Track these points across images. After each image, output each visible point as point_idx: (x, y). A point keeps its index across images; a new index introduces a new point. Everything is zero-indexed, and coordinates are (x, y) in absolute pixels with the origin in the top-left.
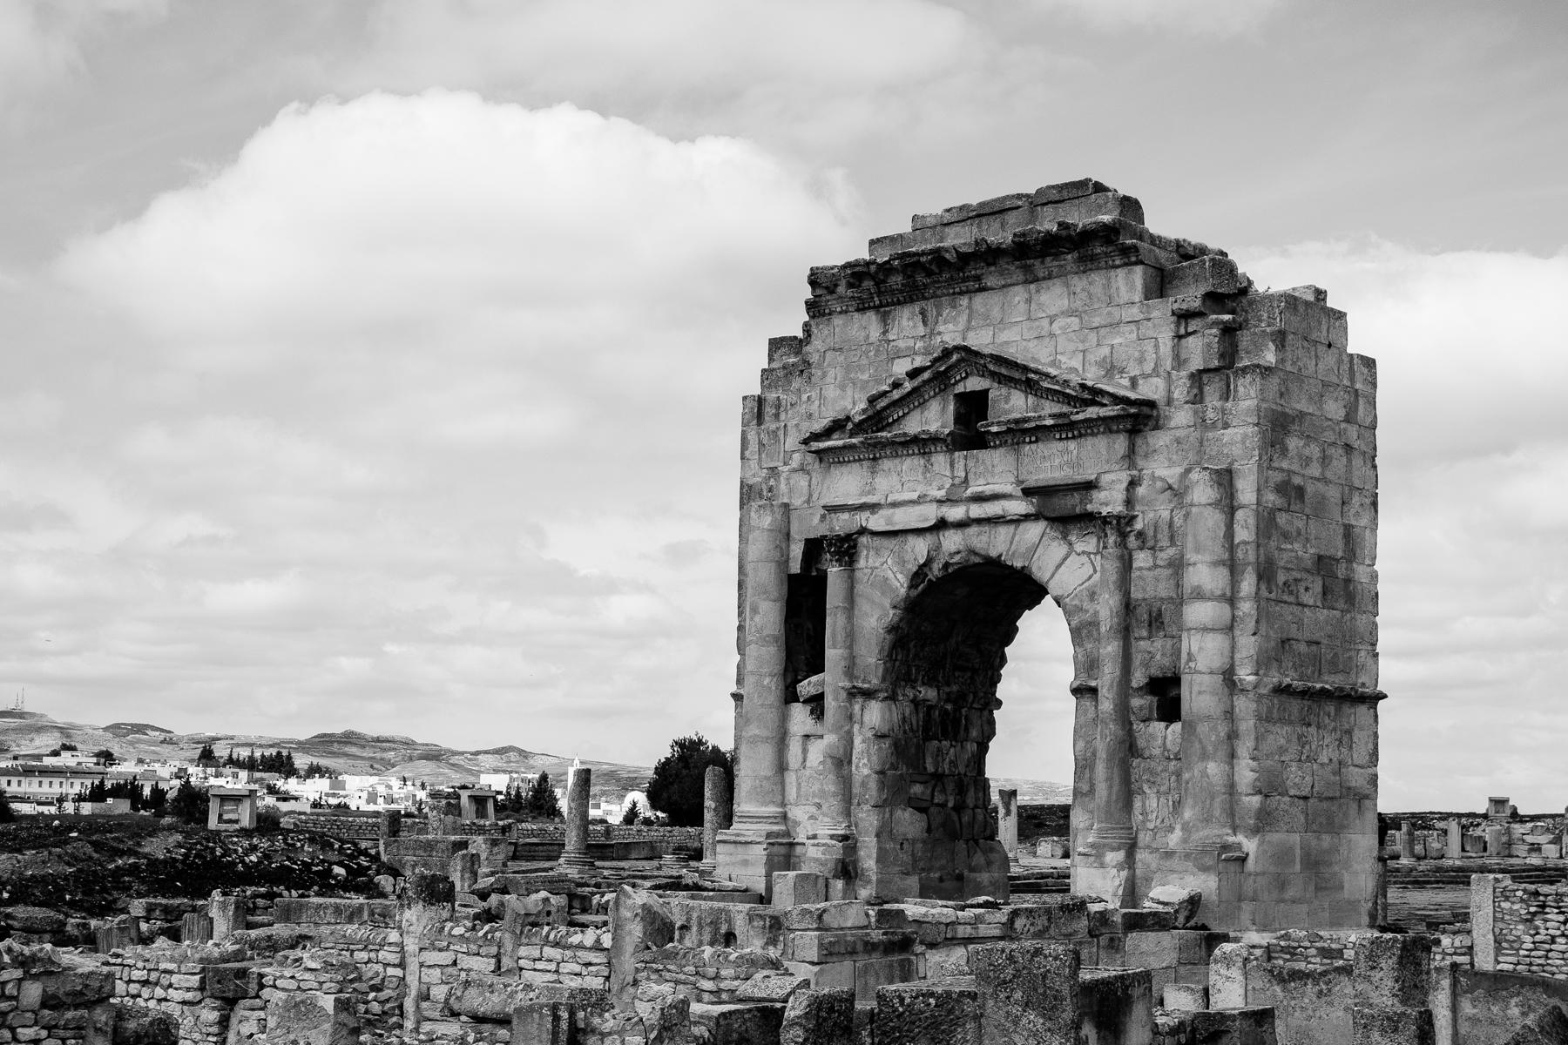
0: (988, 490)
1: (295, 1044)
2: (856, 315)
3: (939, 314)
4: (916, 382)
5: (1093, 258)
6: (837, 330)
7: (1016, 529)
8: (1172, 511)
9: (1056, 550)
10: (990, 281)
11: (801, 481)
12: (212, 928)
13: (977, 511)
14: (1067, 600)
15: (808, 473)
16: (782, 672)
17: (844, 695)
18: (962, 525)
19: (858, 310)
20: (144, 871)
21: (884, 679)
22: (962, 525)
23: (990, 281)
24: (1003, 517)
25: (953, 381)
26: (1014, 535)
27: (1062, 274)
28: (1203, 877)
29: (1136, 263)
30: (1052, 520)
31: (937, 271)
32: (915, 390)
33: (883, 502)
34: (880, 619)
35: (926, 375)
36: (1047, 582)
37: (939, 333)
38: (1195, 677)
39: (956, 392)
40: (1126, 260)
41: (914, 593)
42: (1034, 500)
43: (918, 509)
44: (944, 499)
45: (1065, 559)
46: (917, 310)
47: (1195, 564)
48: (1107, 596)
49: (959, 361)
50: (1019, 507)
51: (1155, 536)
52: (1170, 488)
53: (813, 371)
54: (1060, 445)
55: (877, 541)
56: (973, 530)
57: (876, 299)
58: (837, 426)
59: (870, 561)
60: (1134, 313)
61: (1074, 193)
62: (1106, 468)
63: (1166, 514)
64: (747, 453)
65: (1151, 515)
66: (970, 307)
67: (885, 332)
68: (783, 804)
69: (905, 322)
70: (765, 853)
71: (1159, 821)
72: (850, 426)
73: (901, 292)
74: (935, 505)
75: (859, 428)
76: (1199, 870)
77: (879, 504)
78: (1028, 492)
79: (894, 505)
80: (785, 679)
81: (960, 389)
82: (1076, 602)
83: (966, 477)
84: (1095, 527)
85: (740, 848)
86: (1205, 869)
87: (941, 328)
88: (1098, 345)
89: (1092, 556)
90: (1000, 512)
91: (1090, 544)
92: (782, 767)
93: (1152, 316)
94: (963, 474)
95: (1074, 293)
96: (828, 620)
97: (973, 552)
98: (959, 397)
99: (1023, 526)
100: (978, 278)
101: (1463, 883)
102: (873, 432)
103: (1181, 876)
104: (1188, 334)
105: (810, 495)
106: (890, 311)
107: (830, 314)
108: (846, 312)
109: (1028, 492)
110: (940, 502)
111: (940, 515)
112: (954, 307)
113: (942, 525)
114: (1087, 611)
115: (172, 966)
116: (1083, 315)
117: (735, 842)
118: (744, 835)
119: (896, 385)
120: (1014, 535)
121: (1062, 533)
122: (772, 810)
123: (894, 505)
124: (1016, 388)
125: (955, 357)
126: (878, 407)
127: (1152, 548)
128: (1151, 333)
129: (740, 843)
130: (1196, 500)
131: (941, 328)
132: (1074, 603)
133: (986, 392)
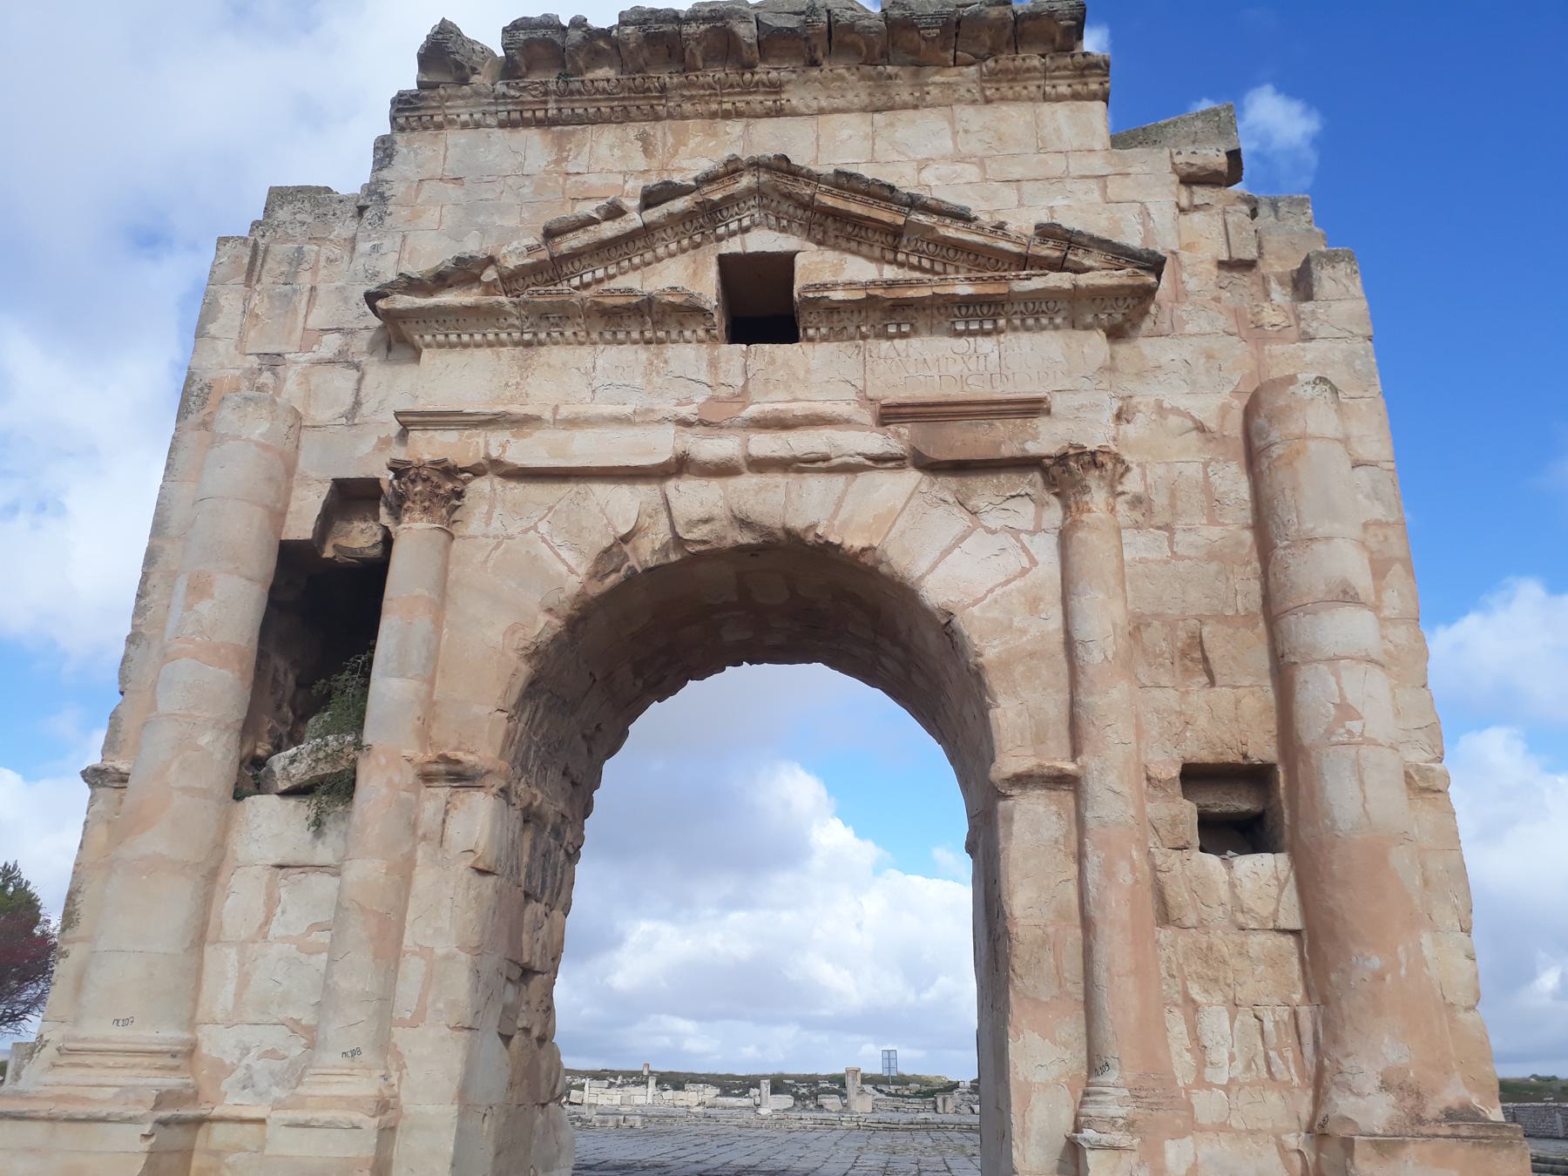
0: (799, 409)
2: (499, 132)
3: (680, 143)
4: (654, 214)
5: (1014, 76)
6: (451, 151)
7: (848, 485)
8: (1206, 465)
9: (946, 522)
10: (795, 97)
11: (341, 382)
13: (766, 444)
14: (976, 610)
15: (357, 367)
16: (239, 725)
17: (410, 775)
18: (723, 470)
19: (502, 125)
20: (14, 975)
21: (502, 756)
22: (723, 470)
23: (795, 97)
24: (826, 459)
25: (721, 230)
26: (845, 493)
27: (949, 100)
29: (1093, 97)
30: (932, 467)
31: (701, 67)
32: (647, 230)
33: (547, 415)
34: (512, 630)
35: (680, 204)
36: (922, 577)
38: (1364, 750)
40: (1079, 88)
41: (596, 589)
43: (628, 435)
44: (693, 419)
45: (963, 538)
47: (1328, 539)
48: (1101, 596)
49: (751, 192)
50: (875, 442)
51: (1173, 506)
52: (1201, 428)
53: (391, 209)
55: (517, 490)
56: (748, 482)
57: (552, 105)
58: (463, 272)
59: (496, 523)
60: (1097, 164)
62: (1067, 383)
63: (1193, 471)
64: (212, 329)
65: (1160, 470)
68: (191, 1023)
69: (603, 150)
70: (146, 1145)
71: (1239, 1064)
73: (609, 95)
74: (671, 429)
75: (511, 281)
77: (538, 419)
78: (889, 415)
79: (573, 423)
80: (241, 747)
81: (733, 246)
82: (995, 613)
84: (1032, 484)
85: (67, 1133)
88: (1020, 205)
89: (1023, 537)
91: (1024, 514)
92: (201, 935)
93: (1130, 170)
97: (744, 523)
98: (722, 259)
99: (863, 478)
100: (776, 88)
101: (1545, 1161)
104: (1197, 208)
105: (357, 404)
107: (440, 127)
108: (478, 125)
109: (889, 415)
110: (685, 423)
111: (680, 450)
113: (681, 466)
117: (51, 1119)
118: (85, 1100)
119: (615, 211)
120: (845, 493)
122: (169, 1034)
123: (573, 423)
125: (746, 181)
127: (1167, 527)
129: (71, 1120)
130: (1312, 428)
132: (990, 615)
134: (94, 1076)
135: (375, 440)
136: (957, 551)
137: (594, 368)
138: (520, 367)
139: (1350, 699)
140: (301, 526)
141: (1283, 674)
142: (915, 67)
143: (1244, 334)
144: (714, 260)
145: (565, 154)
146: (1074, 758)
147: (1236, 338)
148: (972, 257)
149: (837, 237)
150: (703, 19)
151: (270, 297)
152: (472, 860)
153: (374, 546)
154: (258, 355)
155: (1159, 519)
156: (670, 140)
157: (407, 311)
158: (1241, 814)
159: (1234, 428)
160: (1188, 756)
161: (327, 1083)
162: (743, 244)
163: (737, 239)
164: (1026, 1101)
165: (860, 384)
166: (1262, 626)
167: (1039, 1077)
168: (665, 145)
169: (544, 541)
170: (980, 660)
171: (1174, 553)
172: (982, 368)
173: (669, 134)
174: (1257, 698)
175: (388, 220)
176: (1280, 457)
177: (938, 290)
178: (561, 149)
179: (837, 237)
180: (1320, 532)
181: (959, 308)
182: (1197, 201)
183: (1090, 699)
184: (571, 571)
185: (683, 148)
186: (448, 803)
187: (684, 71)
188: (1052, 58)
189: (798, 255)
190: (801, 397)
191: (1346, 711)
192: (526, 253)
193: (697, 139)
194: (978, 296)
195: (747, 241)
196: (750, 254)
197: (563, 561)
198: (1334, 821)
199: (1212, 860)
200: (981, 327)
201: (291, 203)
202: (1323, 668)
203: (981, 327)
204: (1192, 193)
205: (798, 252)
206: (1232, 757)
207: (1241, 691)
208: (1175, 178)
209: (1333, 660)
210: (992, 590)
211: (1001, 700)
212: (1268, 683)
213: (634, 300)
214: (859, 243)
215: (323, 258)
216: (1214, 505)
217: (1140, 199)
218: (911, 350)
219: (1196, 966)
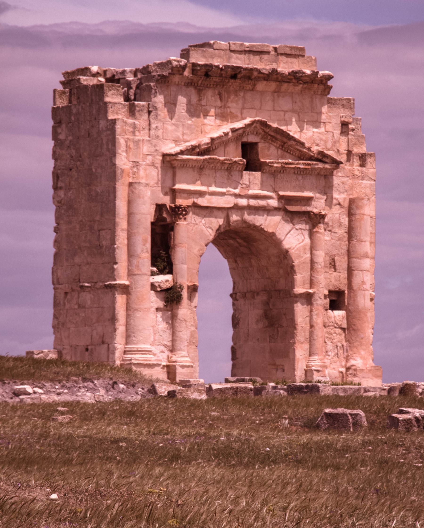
1: (372, 527)
3: (229, 97)
9: (288, 227)
13: (253, 202)
28: (376, 380)
30: (286, 211)
37: (229, 107)
42: (283, 201)
45: (290, 231)
46: (217, 92)
53: (159, 113)
61: (298, 53)
67: (200, 100)
76: (375, 377)
84: (306, 217)
86: (377, 376)
87: (230, 104)
90: (266, 205)
93: (332, 121)
95: (296, 102)
103: (367, 379)
112: (236, 95)
113: (236, 208)
114: (302, 257)
116: (300, 114)
121: (290, 218)
124: (273, 145)
128: (331, 130)
132: (296, 252)
133: (256, 144)
134: (148, 356)
136: (289, 234)
138: (199, 175)
139: (365, 281)
140: (153, 221)
141: (350, 271)
142: (278, 83)
143: (350, 177)
144: (240, 143)
146: (311, 287)
147: (348, 178)
151: (133, 142)
154: (133, 162)
155: (330, 228)
156: (226, 96)
157: (181, 159)
159: (346, 204)
160: (330, 289)
161: (146, 354)
162: (247, 139)
164: (298, 362)
165: (274, 186)
166: (346, 258)
167: (301, 357)
168: (225, 97)
169: (204, 225)
170: (293, 264)
173: (226, 93)
174: (344, 275)
175: (159, 117)
176: (358, 219)
180: (364, 240)
183: (317, 277)
184: (210, 235)
191: (363, 283)
195: (248, 138)
197: (208, 231)
198: (358, 306)
201: (111, 90)
202: (360, 272)
207: (341, 274)
209: (362, 271)
210: (296, 246)
211: (297, 274)
212: (346, 272)
213: (231, 162)
215: (141, 128)
216: (341, 225)
217: (333, 131)
219: (327, 335)
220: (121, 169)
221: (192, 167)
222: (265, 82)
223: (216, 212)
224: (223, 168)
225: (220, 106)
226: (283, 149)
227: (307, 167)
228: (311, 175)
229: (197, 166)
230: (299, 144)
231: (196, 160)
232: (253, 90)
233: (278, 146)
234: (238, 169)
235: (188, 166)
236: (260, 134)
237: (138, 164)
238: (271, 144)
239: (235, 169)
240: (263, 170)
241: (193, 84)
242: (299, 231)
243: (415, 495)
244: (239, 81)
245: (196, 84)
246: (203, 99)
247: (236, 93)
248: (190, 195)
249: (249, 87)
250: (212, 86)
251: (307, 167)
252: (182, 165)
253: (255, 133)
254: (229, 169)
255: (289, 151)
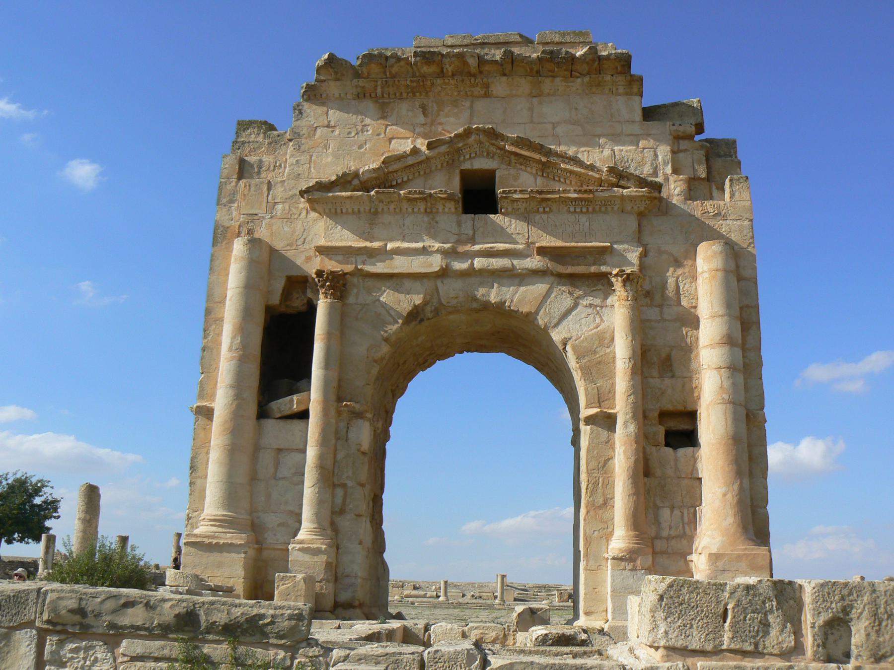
12: (540, 304)
37: (441, 124)
39: (462, 168)
46: (417, 104)
54: (572, 218)
66: (471, 107)
72: (356, 182)
81: (467, 166)
83: (474, 233)
94: (471, 232)
95: (576, 109)
96: (44, 434)
102: (385, 188)
104: (681, 151)
106: (390, 103)
115: (430, 617)
124: (526, 171)
126: (391, 169)
131: (443, 120)
135: (304, 258)
137: (404, 225)
138: (370, 224)
140: (276, 300)
144: (458, 172)
145: (385, 114)
148: (577, 177)
149: (516, 163)
150: (481, 651)
152: (811, 665)
153: (303, 305)
156: (436, 108)
158: (687, 430)
162: (472, 165)
163: (469, 162)
171: (662, 318)
172: (581, 229)
173: (435, 105)
177: (562, 195)
178: (383, 112)
179: (516, 163)
181: (572, 202)
182: (682, 148)
185: (442, 113)
186: (348, 424)
187: (443, 77)
188: (616, 77)
189: (497, 170)
190: (499, 241)
192: (373, 172)
193: (449, 108)
194: (579, 198)
196: (476, 170)
199: (669, 450)
200: (581, 210)
203: (581, 210)
204: (679, 144)
205: (498, 169)
206: (680, 408)
208: (671, 137)
214: (526, 166)
218: (549, 220)
220: (223, 226)
221: (353, 213)
222: (504, 79)
223: (407, 283)
224: (416, 210)
225: (423, 122)
226: (544, 175)
227: (586, 196)
228: (606, 212)
229: (362, 209)
230: (567, 161)
231: (350, 197)
232: (487, 95)
233: (534, 171)
234: (446, 210)
235: (344, 211)
236: (494, 154)
237: (256, 217)
238: (521, 169)
239: (440, 210)
240: (501, 209)
241: (367, 95)
242: (590, 310)
243: (621, 90)
244: (452, 82)
245: (373, 95)
246: (391, 116)
247: (455, 104)
248: (348, 258)
249: (479, 91)
250: (405, 95)
251: (586, 196)
252: (333, 211)
253: (485, 154)
254: (428, 210)
255: (557, 179)
